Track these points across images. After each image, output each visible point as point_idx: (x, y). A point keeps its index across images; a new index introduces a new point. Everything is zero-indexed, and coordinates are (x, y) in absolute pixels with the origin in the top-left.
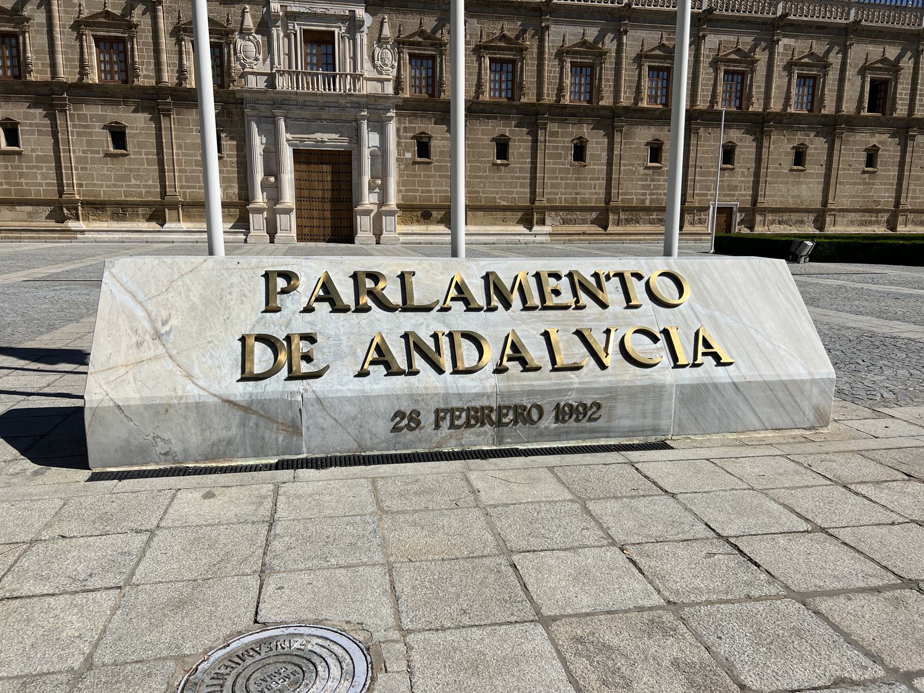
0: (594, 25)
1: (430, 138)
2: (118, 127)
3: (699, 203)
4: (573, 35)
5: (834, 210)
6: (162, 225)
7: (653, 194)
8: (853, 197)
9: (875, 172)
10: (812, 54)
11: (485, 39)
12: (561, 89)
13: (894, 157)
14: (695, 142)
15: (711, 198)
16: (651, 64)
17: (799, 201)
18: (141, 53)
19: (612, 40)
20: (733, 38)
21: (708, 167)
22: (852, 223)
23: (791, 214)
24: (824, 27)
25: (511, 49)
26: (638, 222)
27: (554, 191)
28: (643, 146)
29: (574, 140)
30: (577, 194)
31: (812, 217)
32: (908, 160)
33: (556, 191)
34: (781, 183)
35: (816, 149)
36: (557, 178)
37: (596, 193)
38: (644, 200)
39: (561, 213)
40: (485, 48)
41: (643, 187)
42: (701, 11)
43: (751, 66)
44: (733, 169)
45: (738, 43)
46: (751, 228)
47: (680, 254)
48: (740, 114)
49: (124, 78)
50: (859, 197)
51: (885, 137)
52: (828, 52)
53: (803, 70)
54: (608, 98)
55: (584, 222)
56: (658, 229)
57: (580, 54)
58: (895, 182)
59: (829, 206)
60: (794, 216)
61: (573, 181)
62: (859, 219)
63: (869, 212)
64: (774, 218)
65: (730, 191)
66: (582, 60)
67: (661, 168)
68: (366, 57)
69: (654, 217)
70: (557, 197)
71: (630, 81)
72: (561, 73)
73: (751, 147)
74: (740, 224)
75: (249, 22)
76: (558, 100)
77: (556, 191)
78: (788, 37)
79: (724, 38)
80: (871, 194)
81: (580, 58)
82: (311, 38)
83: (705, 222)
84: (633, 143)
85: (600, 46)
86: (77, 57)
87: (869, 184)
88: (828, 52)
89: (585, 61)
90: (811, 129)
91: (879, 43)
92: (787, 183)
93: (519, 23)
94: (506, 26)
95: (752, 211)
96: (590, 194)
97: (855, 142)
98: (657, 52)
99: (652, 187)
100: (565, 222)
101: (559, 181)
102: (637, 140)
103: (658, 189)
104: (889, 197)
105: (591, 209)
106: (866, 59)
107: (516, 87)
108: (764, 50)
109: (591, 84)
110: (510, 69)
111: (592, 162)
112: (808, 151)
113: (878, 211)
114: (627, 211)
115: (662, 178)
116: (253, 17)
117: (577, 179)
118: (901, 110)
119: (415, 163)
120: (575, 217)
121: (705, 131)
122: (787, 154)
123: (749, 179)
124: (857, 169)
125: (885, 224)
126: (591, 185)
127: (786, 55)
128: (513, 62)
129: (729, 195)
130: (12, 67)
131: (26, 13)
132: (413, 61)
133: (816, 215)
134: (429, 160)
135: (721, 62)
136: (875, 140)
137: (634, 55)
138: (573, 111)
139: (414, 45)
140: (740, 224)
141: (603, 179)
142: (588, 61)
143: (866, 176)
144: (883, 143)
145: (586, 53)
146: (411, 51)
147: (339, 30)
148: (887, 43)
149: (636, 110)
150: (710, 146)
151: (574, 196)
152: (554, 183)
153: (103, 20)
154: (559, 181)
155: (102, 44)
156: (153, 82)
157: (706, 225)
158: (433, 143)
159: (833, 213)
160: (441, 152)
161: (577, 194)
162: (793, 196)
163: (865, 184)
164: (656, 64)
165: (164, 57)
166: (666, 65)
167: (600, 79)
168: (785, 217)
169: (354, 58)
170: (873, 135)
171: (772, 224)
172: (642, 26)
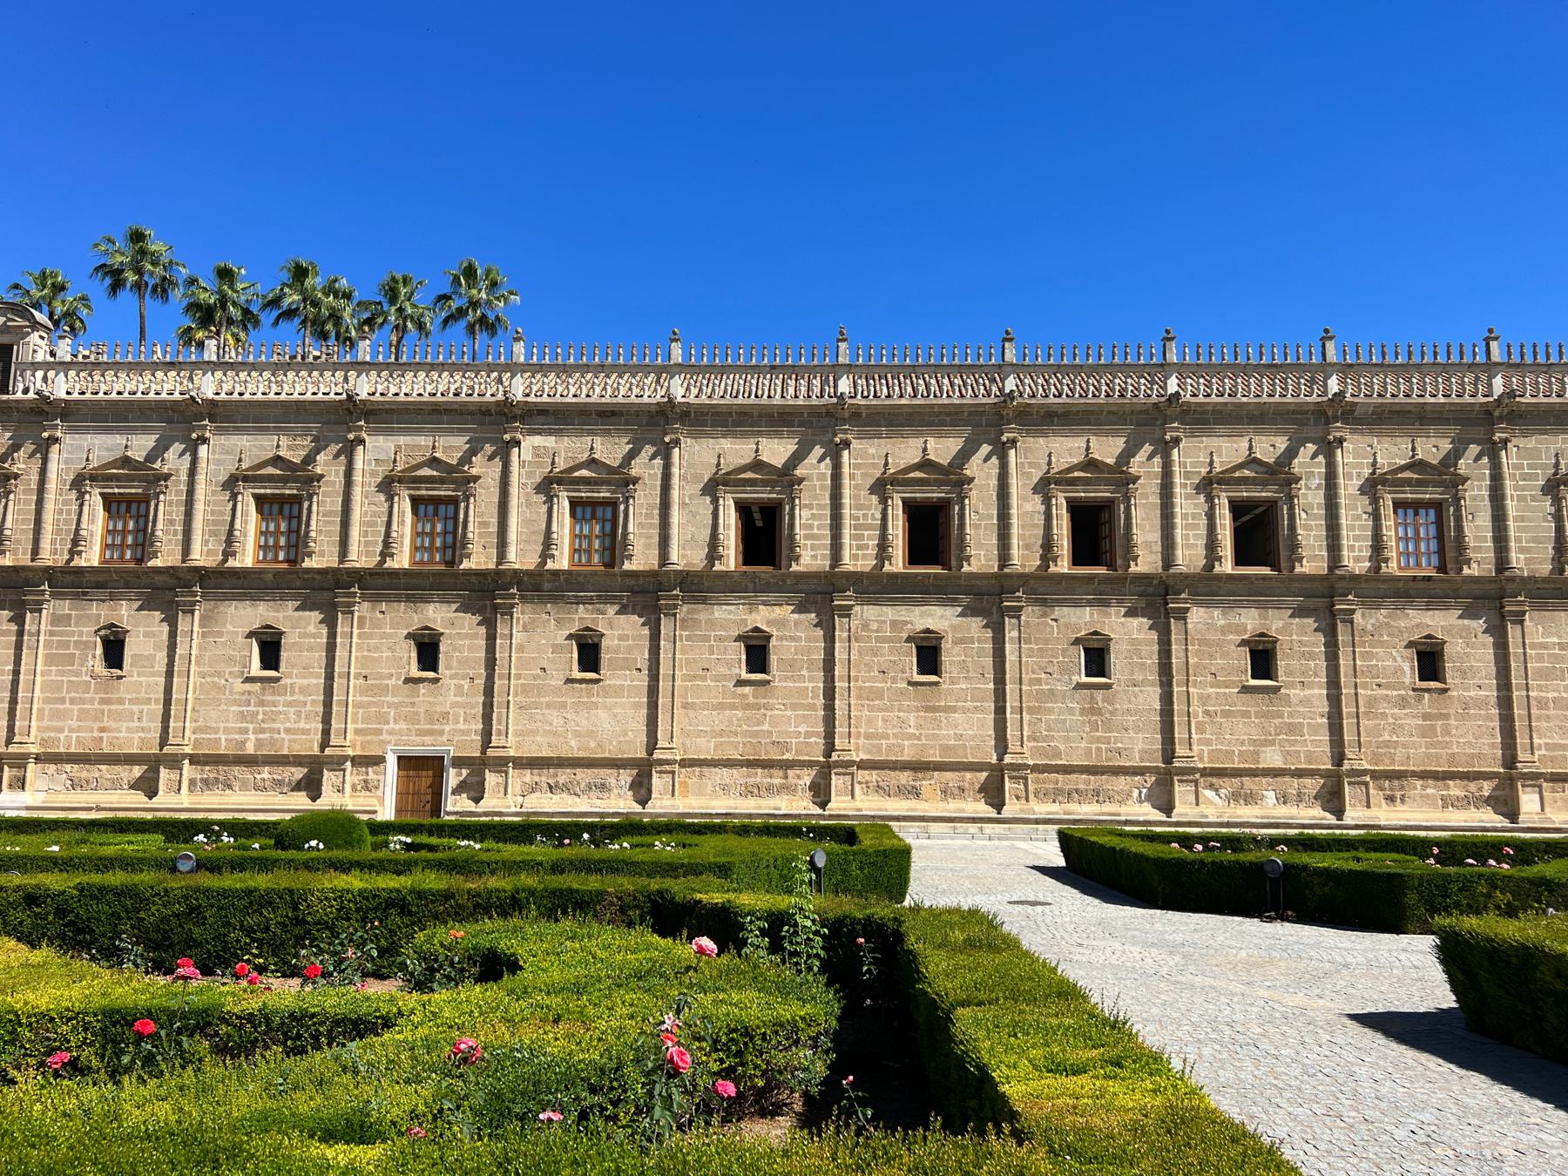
0: (145, 431)
2: (1432, 644)
3: (363, 748)
4: (108, 449)
5: (668, 762)
6: (477, 800)
7: (262, 731)
8: (722, 733)
9: (768, 682)
10: (594, 461)
12: (1212, 545)
13: (809, 651)
14: (1015, 634)
15: (389, 738)
16: (257, 491)
17: (593, 744)
18: (479, 516)
19: (181, 455)
20: (424, 441)
21: (380, 676)
22: (1447, 803)
23: (578, 771)
24: (614, 413)
25: (939, 483)
26: (230, 787)
27: (55, 724)
28: (240, 639)
29: (99, 630)
30: (102, 730)
31: (627, 776)
33: (60, 724)
34: (548, 706)
35: (622, 638)
36: (63, 700)
37: (143, 729)
38: (243, 743)
39: (68, 767)
41: (242, 717)
42: (1491, 399)
43: (1286, 489)
44: (436, 680)
45: (434, 447)
46: (1339, 812)
48: (1442, 581)
49: (139, 555)
50: (736, 734)
51: (785, 612)
52: (1291, 453)
53: (579, 491)
54: (1312, 558)
55: (115, 785)
56: (271, 800)
57: (118, 481)
58: (821, 701)
59: (1523, 768)
60: (584, 776)
61: (96, 706)
62: (743, 781)
63: (764, 767)
64: (537, 779)
65: (432, 723)
66: (122, 491)
67: (277, 680)
69: (266, 775)
70: (62, 736)
71: (369, 524)
73: (475, 636)
74: (457, 791)
76: (1209, 567)
77: (60, 724)
78: (540, 434)
79: (403, 440)
80: (766, 727)
81: (427, 489)
83: (377, 788)
84: (220, 634)
85: (466, 468)
87: (758, 707)
88: (631, 456)
89: (431, 493)
90: (610, 600)
91: (744, 435)
92: (563, 705)
93: (8, 435)
95: (478, 768)
96: (129, 730)
97: (712, 624)
98: (270, 470)
99: (260, 717)
100: (74, 785)
101: (67, 705)
102: (230, 627)
103: (274, 721)
104: (808, 734)
105: (130, 760)
106: (718, 465)
107: (615, 547)
108: (491, 458)
109: (1440, 537)
110: (609, 515)
111: (135, 671)
112: (604, 643)
113: (786, 765)
114: (206, 763)
115: (282, 699)
117: (104, 701)
118: (1146, 561)
120: (97, 775)
121: (373, 609)
123: (474, 700)
124: (725, 678)
125: (809, 794)
126: (132, 713)
127: (539, 465)
128: (613, 504)
129: (431, 732)
131: (968, 472)
132: (1400, 511)
133: (635, 772)
134: (1443, 686)
135: (399, 482)
137: (223, 477)
138: (101, 578)
139: (432, 483)
140: (457, 791)
141: (157, 701)
142: (133, 491)
143: (747, 690)
144: (781, 623)
145: (441, 481)
146: (412, 492)
148: (760, 434)
149: (221, 572)
150: (384, 636)
151: (96, 734)
152: (58, 710)
153: (1082, 474)
154: (67, 705)
155: (1400, 511)
156: (653, 563)
157: (379, 793)
159: (668, 768)
161: (102, 730)
162: (577, 734)
163: (748, 707)
164: (268, 491)
166: (287, 492)
168: (563, 776)
170: (752, 607)
171: (533, 792)
172: (238, 429)
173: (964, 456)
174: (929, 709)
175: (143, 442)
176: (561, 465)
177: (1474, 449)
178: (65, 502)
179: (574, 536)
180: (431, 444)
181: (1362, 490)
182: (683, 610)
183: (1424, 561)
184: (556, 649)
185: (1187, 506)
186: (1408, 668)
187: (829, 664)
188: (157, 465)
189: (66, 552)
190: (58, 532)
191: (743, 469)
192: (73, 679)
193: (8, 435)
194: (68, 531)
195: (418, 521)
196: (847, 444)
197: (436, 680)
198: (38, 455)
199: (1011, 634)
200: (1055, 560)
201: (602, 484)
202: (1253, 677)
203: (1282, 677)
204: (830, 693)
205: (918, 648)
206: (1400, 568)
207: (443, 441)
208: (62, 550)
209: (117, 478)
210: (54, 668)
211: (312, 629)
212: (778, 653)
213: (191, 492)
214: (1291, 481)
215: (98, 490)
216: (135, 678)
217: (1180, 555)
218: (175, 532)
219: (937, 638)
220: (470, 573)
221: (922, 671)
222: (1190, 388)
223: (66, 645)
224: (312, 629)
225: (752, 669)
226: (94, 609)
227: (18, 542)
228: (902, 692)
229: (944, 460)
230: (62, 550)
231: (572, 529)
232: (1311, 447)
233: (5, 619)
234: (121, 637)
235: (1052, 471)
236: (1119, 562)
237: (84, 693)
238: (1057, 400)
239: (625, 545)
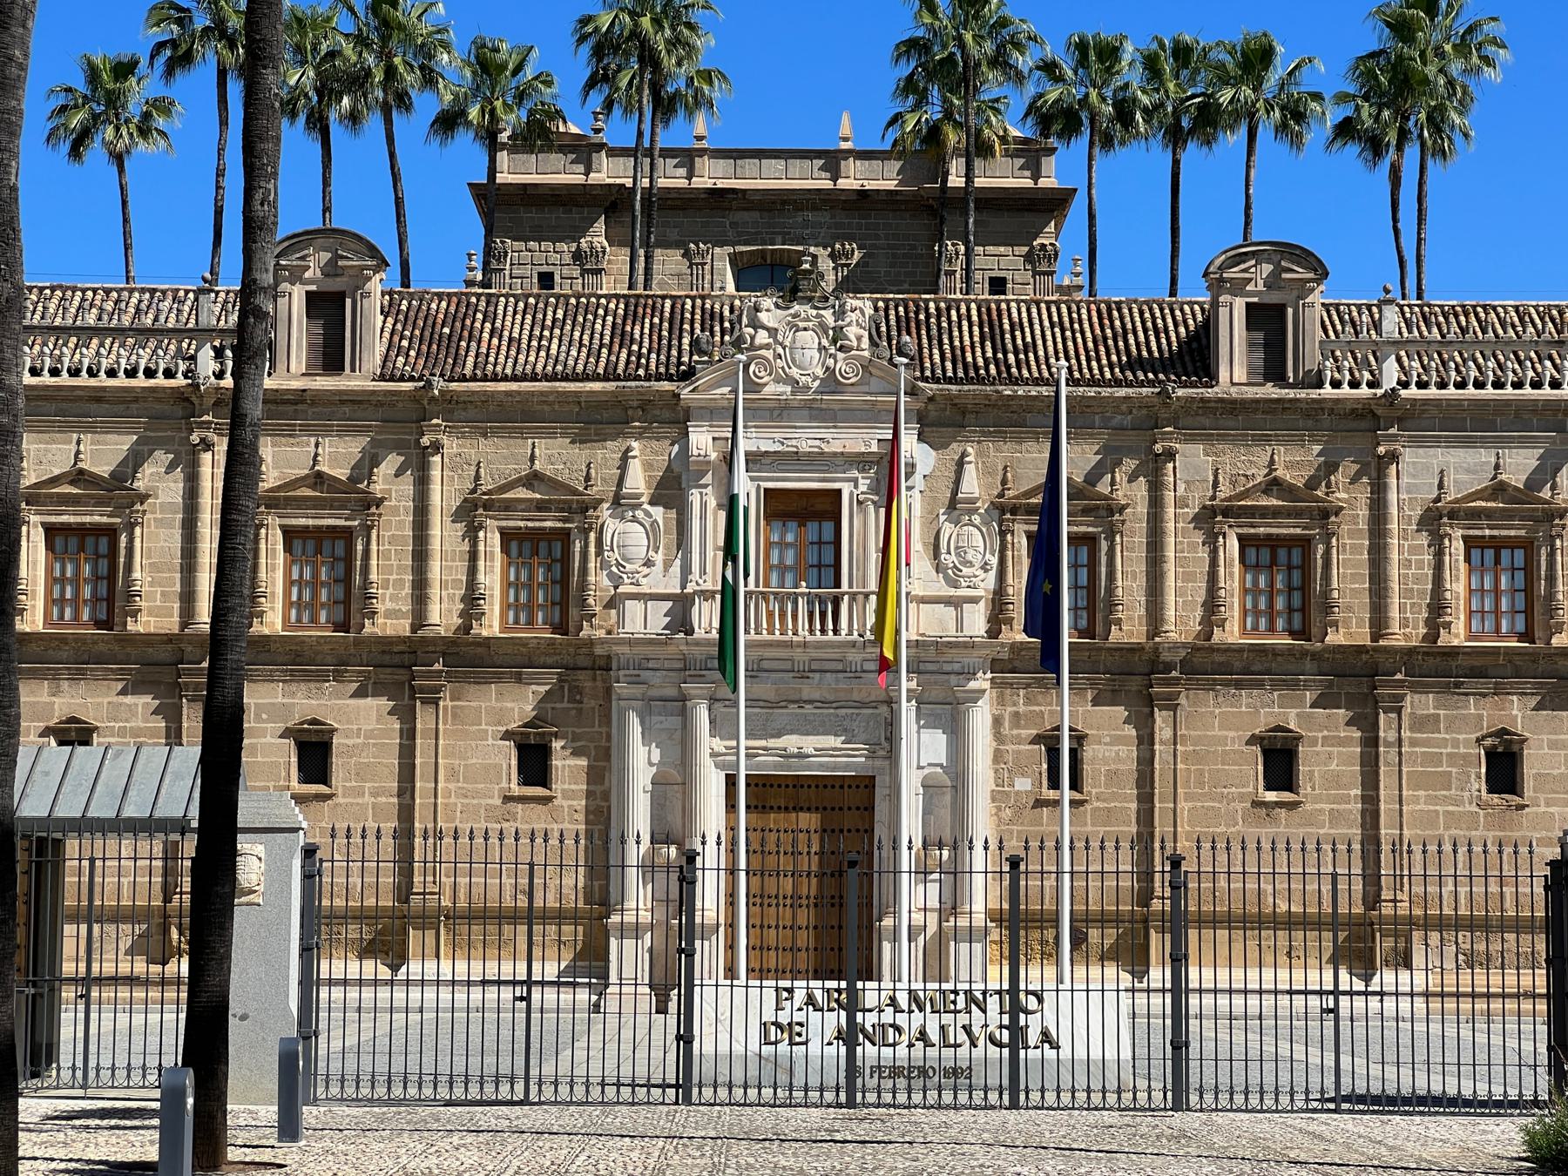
0: (1524, 443)
11: (1225, 491)
12: (1212, 605)
29: (1484, 738)
40: (1226, 512)
57: (1489, 517)
66: (1495, 533)
72: (1438, 567)
81: (1491, 527)
93: (1317, 448)
111: (1542, 797)
116: (648, 466)
142: (1513, 533)
147: (853, 488)
173: (135, 460)
175: (1520, 460)
176: (487, 484)
177: (1130, 464)
178: (1414, 550)
179: (51, 580)
180: (1493, 460)
181: (457, 516)
183: (1280, 623)
185: (1181, 544)
188: (1546, 493)
189: (1421, 624)
190: (1406, 593)
191: (54, 481)
192: (1451, 808)
193: (1317, 448)
194: (1422, 593)
195: (293, 562)
196: (437, 447)
197: (549, 799)
198: (1365, 480)
200: (1222, 624)
201: (1511, 518)
202: (1268, 788)
203: (1305, 788)
205: (1265, 752)
206: (1244, 631)
207: (1283, 455)
208: (1416, 621)
209: (1488, 514)
210: (1422, 793)
212: (1308, 766)
214: (369, 503)
215: (1460, 533)
216: (1542, 809)
217: (435, 614)
218: (1423, 592)
219: (1295, 738)
220: (148, 639)
222: (1511, 374)
223: (1435, 759)
225: (306, 778)
226: (1472, 707)
227: (1349, 609)
229: (104, 470)
230: (1416, 621)
231: (49, 570)
232: (1130, 464)
233: (1342, 721)
234: (1515, 748)
235: (1220, 495)
236: (1314, 630)
237: (1228, 826)
238: (35, 381)
239: (1111, 606)
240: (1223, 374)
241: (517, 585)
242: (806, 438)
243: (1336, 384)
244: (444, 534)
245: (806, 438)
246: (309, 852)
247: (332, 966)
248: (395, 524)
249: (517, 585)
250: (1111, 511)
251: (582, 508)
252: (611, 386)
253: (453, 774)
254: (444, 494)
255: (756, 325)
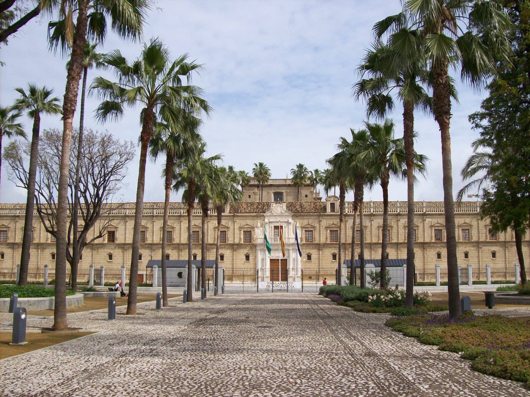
1: (311, 254)
11: (328, 225)
12: (240, 239)
32: (480, 255)
40: (328, 227)
47: (279, 260)
68: (292, 232)
72: (379, 233)
75: (259, 225)
82: (276, 227)
86: (213, 236)
94: (334, 221)
116: (260, 223)
119: (307, 262)
122: (434, 255)
130: (197, 237)
136: (467, 249)
137: (376, 227)
143: (465, 261)
147: (284, 225)
158: (312, 256)
160: (315, 259)
165: (236, 236)
167: (418, 234)
169: (288, 233)
174: (494, 263)
176: (433, 224)
182: (428, 250)
184: (434, 255)
186: (244, 257)
187: (479, 257)
199: (507, 251)
204: (479, 261)
211: (393, 252)
213: (371, 230)
221: (493, 257)
224: (393, 252)
225: (493, 257)
226: (106, 250)
228: (490, 261)
240: (327, 211)
241: (245, 237)
242: (279, 219)
243: (366, 212)
244: (237, 231)
245: (279, 219)
246: (223, 270)
247: (304, 282)
248: (231, 230)
249: (332, 237)
250: (314, 227)
251: (253, 228)
252: (256, 214)
253: (238, 259)
254: (427, 226)
255: (273, 206)
